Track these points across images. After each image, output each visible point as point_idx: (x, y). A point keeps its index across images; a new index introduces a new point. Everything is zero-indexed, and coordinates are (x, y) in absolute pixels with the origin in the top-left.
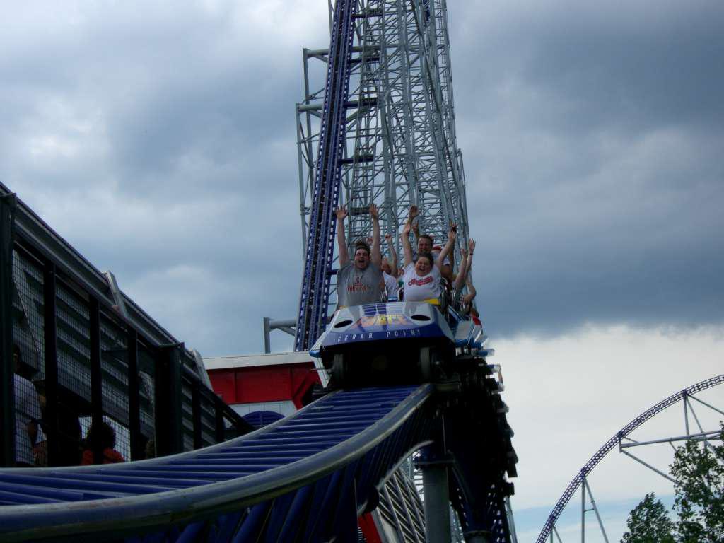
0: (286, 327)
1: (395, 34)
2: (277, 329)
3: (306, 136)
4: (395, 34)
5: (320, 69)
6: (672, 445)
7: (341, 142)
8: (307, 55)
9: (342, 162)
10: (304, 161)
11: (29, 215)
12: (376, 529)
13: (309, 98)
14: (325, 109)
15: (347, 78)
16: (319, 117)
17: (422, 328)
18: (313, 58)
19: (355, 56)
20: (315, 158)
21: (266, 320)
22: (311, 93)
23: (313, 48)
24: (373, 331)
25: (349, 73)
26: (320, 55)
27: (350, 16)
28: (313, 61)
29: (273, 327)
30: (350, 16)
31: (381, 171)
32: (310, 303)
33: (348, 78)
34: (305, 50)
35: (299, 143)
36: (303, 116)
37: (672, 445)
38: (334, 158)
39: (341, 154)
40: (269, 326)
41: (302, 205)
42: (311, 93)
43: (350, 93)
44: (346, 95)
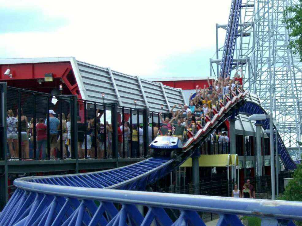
0: (224, 27)
2: (220, 28)
5: (223, 34)
6: (286, 140)
8: (218, 27)
11: (277, 180)
12: (141, 224)
14: (228, 26)
16: (226, 30)
17: (173, 146)
21: (217, 25)
24: (199, 181)
29: (219, 27)
31: (267, 41)
32: (234, 13)
34: (217, 25)
37: (286, 140)
38: (235, 24)
39: (238, 22)
40: (218, 27)
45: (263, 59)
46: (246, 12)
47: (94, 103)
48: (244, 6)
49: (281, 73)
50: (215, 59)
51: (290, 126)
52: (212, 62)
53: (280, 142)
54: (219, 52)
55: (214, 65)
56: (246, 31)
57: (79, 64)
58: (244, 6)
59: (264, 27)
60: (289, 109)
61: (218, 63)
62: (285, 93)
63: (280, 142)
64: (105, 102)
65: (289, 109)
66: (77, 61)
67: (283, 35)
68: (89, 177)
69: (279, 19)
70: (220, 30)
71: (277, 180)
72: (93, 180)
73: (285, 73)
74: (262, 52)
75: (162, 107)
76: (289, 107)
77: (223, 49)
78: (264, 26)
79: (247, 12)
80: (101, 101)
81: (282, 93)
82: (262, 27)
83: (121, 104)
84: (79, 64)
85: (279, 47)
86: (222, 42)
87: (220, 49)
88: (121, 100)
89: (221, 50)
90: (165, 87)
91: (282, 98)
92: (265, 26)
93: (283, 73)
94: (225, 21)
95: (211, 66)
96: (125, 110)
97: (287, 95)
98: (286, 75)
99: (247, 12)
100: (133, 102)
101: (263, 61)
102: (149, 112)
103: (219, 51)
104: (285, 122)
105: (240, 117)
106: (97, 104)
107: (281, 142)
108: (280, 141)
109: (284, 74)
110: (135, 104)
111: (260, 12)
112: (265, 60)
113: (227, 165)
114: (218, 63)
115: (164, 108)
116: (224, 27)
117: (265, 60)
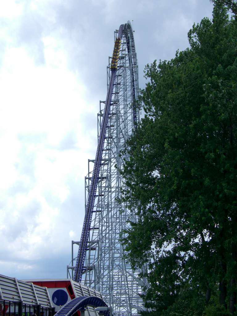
1: (115, 172)
3: (88, 186)
4: (115, 172)
5: (77, 248)
7: (107, 122)
8: (73, 243)
9: (95, 196)
10: (86, 191)
13: (101, 111)
15: (85, 252)
18: (91, 162)
19: (112, 103)
20: (110, 76)
22: (101, 110)
23: (75, 241)
25: (112, 96)
26: (77, 243)
27: (91, 211)
28: (75, 245)
30: (91, 211)
32: (90, 203)
33: (104, 144)
35: (86, 187)
36: (115, 33)
41: (107, 84)
42: (101, 110)
43: (94, 206)
44: (111, 99)
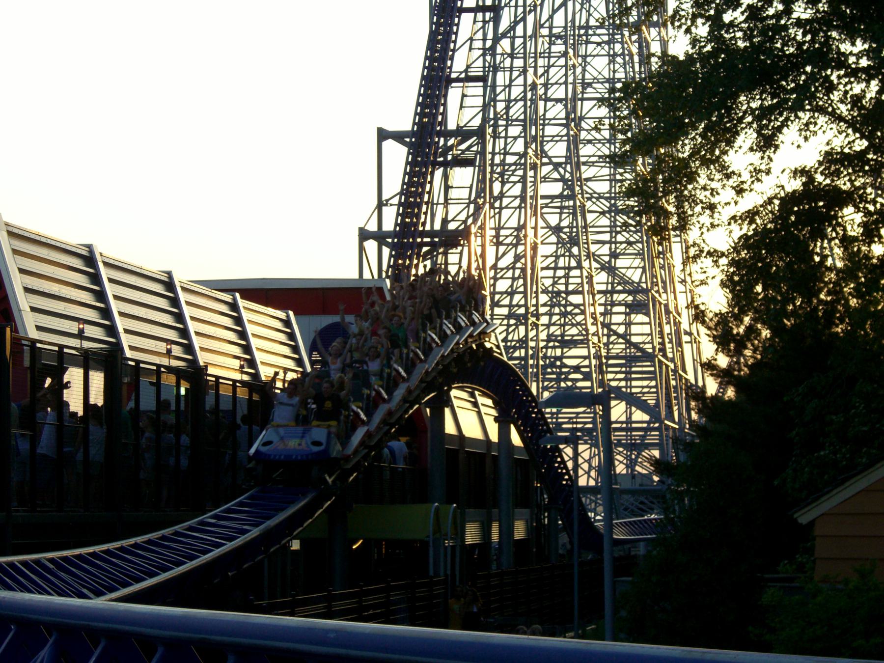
0: (398, 137)
8: (383, 135)
29: (386, 138)
40: (383, 135)
45: (503, 232)
46: (464, 96)
47: (231, 383)
48: (458, 80)
49: (550, 273)
50: (373, 227)
51: (575, 426)
52: (364, 235)
53: (560, 471)
54: (384, 208)
55: (371, 246)
56: (463, 152)
57: (11, 234)
58: (458, 80)
59: (506, 141)
60: (572, 376)
61: (380, 237)
62: (558, 333)
63: (560, 471)
64: (87, 345)
65: (572, 376)
66: (7, 224)
67: (560, 164)
68: (51, 566)
69: (550, 120)
70: (390, 145)
71: (457, 560)
72: (63, 575)
73: (560, 273)
74: (500, 213)
75: (81, 326)
76: (574, 372)
77: (396, 200)
78: (506, 137)
79: (466, 96)
80: (75, 342)
81: (550, 333)
82: (502, 141)
83: (33, 334)
84: (11, 234)
85: (550, 200)
86: (394, 184)
87: (387, 201)
88: (126, 340)
89: (391, 205)
90: (246, 306)
91: (551, 344)
92: (509, 140)
93: (555, 273)
94: (405, 121)
95: (362, 249)
96: (221, 387)
97: (566, 338)
98: (563, 281)
99: (466, 96)
100: (73, 328)
101: (501, 239)
102: (209, 378)
103: (386, 205)
104: (557, 414)
105: (121, 329)
106: (221, 381)
107: (564, 471)
108: (562, 469)
109: (560, 278)
110: (80, 335)
111: (498, 98)
112: (507, 237)
113: (428, 537)
114: (380, 237)
115: (177, 351)
116: (398, 137)
117: (507, 237)
